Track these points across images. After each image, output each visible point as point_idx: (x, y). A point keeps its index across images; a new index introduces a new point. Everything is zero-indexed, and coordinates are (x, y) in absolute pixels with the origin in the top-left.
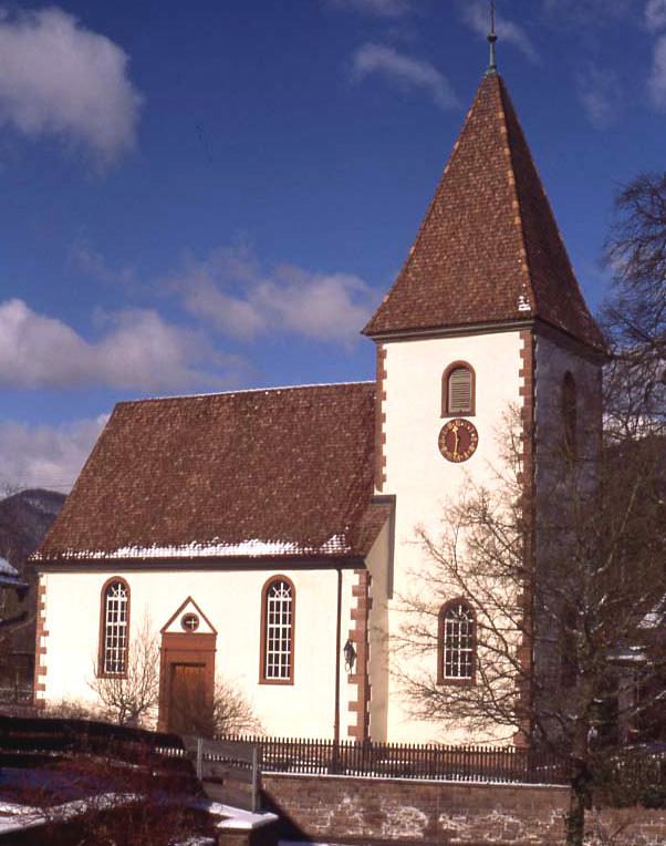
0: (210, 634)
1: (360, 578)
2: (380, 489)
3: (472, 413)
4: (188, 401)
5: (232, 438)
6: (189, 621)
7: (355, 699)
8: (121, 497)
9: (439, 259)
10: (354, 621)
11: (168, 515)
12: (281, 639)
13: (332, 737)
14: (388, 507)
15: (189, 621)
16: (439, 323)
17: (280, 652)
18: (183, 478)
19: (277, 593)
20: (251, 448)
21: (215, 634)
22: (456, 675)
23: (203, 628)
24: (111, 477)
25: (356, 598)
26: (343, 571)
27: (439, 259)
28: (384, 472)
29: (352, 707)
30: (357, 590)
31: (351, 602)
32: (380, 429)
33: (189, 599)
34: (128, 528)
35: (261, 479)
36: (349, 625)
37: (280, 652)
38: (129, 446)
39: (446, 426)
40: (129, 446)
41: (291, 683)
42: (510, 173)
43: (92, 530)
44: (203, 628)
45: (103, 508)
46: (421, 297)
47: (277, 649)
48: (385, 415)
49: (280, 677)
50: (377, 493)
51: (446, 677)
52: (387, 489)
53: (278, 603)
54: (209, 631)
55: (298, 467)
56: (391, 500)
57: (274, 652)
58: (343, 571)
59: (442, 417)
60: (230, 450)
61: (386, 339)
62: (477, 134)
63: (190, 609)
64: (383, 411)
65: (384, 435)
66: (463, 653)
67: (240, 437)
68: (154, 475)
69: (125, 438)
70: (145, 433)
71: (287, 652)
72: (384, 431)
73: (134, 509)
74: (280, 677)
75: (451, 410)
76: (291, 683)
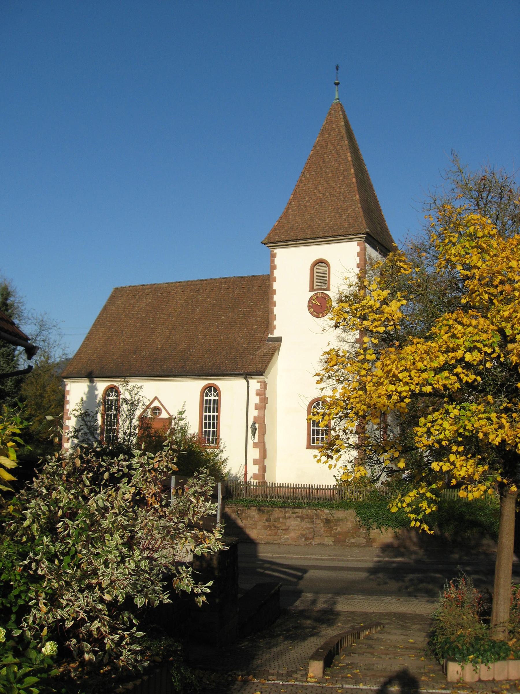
1: (261, 385)
2: (272, 333)
7: (257, 457)
10: (257, 411)
14: (277, 343)
19: (209, 394)
25: (258, 398)
29: (255, 462)
30: (258, 392)
31: (255, 400)
32: (272, 298)
33: (156, 398)
36: (253, 413)
42: (349, 154)
46: (297, 223)
47: (210, 412)
50: (270, 336)
52: (276, 334)
56: (279, 340)
63: (156, 404)
64: (274, 288)
65: (275, 302)
70: (130, 304)
72: (274, 300)
75: (315, 287)
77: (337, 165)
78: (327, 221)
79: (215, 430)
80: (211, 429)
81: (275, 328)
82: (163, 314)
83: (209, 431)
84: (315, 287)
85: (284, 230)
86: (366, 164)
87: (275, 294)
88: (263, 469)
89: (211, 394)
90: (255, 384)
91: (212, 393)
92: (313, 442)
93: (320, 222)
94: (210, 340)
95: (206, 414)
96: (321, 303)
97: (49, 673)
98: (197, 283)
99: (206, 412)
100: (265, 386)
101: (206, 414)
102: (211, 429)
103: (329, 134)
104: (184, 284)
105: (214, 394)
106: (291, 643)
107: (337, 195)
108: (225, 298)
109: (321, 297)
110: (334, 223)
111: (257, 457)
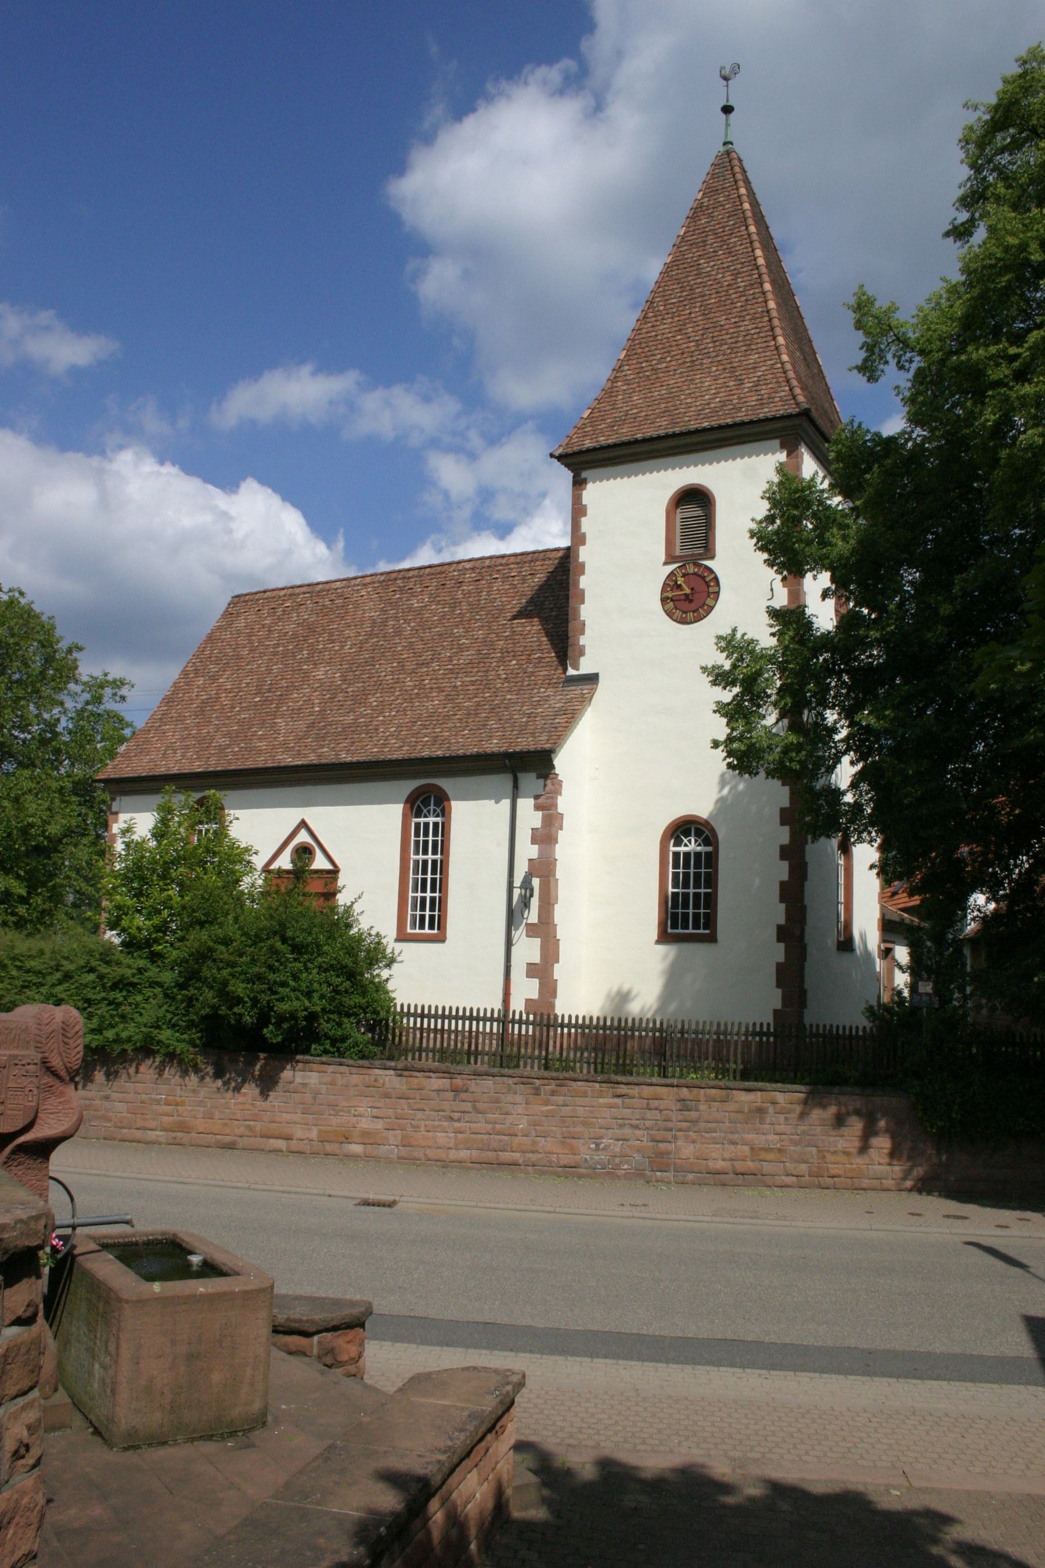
0: (328, 872)
2: (576, 667)
3: (712, 558)
4: (321, 586)
5: (374, 622)
6: (304, 852)
7: (536, 958)
8: (225, 700)
9: (661, 360)
11: (282, 716)
12: (431, 838)
13: (498, 1005)
14: (585, 689)
15: (304, 852)
16: (662, 432)
17: (430, 857)
18: (307, 673)
19: (425, 811)
20: (398, 632)
21: (334, 872)
22: (688, 928)
23: (320, 863)
24: (214, 679)
26: (520, 775)
27: (661, 360)
28: (582, 642)
29: (532, 970)
32: (577, 583)
33: (303, 824)
34: (228, 734)
35: (410, 666)
36: (527, 851)
37: (430, 857)
38: (241, 640)
39: (672, 573)
40: (241, 640)
41: (441, 939)
43: (183, 739)
44: (320, 863)
45: (201, 711)
46: (635, 406)
47: (425, 852)
48: (584, 646)
49: (427, 931)
51: (669, 930)
53: (426, 825)
54: (328, 866)
55: (461, 649)
57: (421, 857)
58: (520, 775)
59: (666, 563)
60: (370, 635)
61: (587, 462)
62: (710, 216)
63: (303, 837)
64: (581, 560)
65: (583, 592)
66: (697, 896)
67: (386, 620)
68: (269, 671)
69: (239, 632)
70: (263, 626)
71: (438, 857)
72: (582, 586)
73: (239, 713)
74: (427, 931)
76: (441, 939)
77: (729, 278)
78: (707, 397)
79: (437, 895)
80: (428, 894)
81: (582, 653)
82: (333, 642)
83: (697, 885)
84: (678, 552)
85: (603, 426)
86: (563, 792)
87: (583, 573)
88: (549, 989)
89: (429, 811)
90: (527, 810)
91: (432, 807)
92: (674, 926)
93: (688, 401)
94: (431, 688)
95: (417, 857)
96: (692, 589)
97: (721, 748)
98: (411, 574)
99: (417, 853)
100: (547, 807)
101: (417, 857)
102: (428, 894)
103: (710, 216)
104: (382, 578)
105: (435, 811)
106: (289, 553)
107: (730, 341)
108: (471, 599)
109: (695, 574)
110: (724, 399)
111: (536, 958)
